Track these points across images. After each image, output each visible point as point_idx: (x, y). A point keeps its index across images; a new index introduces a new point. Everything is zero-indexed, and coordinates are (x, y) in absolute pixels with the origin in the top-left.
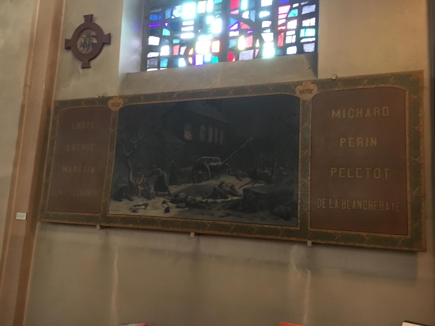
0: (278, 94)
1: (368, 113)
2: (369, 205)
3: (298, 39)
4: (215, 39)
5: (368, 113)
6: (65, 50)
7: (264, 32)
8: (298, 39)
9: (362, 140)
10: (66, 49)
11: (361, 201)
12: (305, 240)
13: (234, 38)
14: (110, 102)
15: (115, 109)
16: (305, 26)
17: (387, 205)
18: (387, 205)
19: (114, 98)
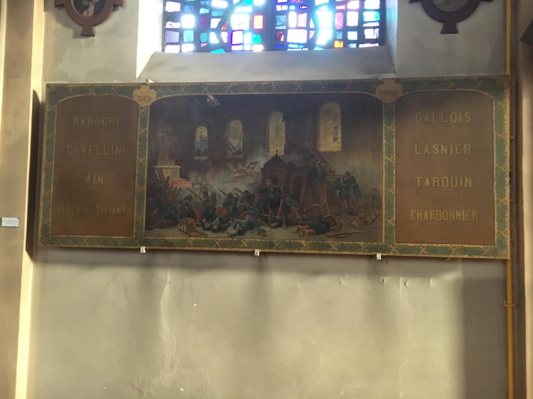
0: (443, 91)
1: (83, 122)
2: (418, 214)
3: (361, 21)
4: (257, 12)
5: (83, 122)
6: (55, 8)
7: (191, 6)
8: (361, 21)
9: (470, 147)
10: (56, 6)
11: (421, 211)
12: (373, 253)
13: (284, 13)
14: (136, 92)
15: (145, 104)
16: (379, 4)
17: (426, 214)
18: (426, 214)
19: (142, 87)
